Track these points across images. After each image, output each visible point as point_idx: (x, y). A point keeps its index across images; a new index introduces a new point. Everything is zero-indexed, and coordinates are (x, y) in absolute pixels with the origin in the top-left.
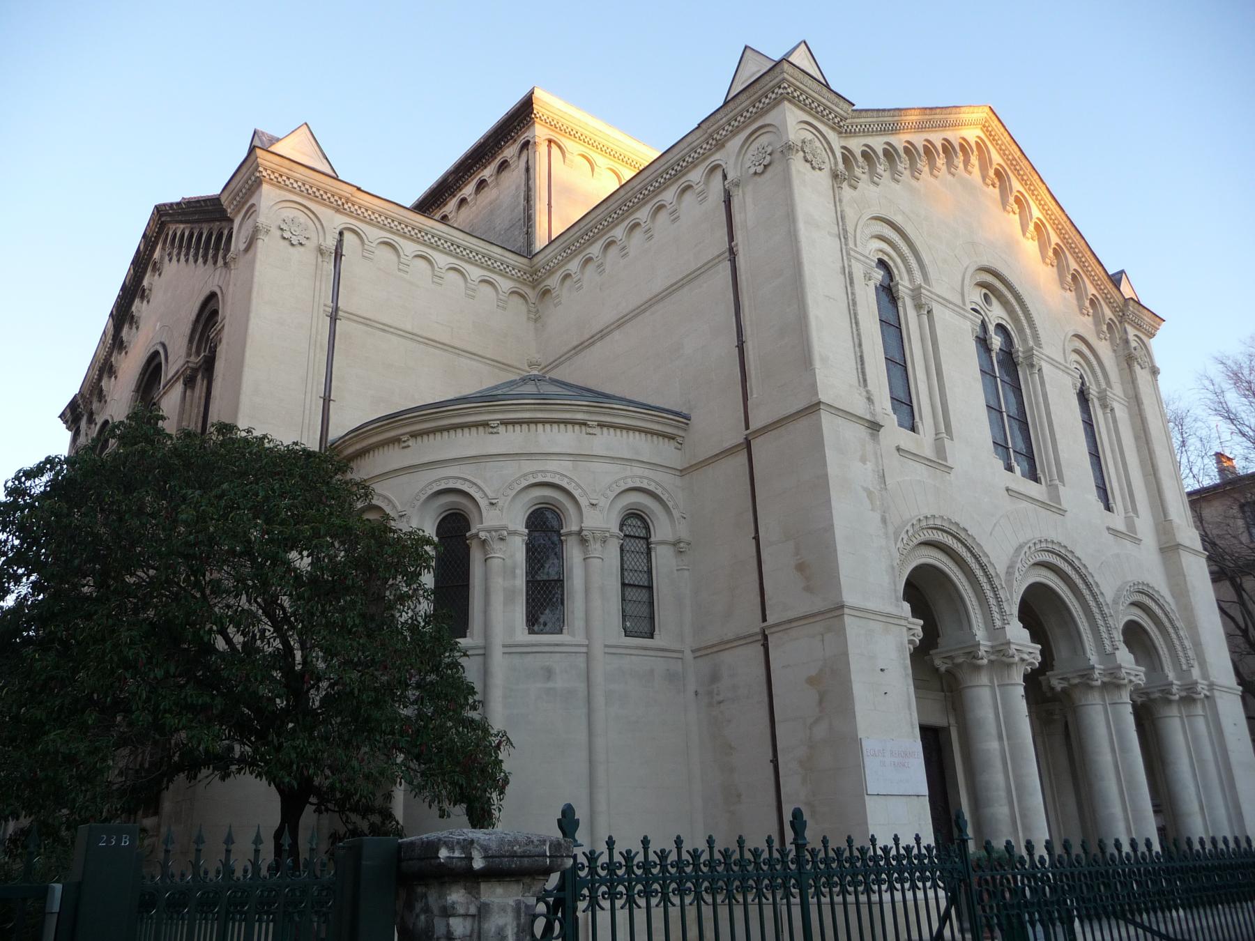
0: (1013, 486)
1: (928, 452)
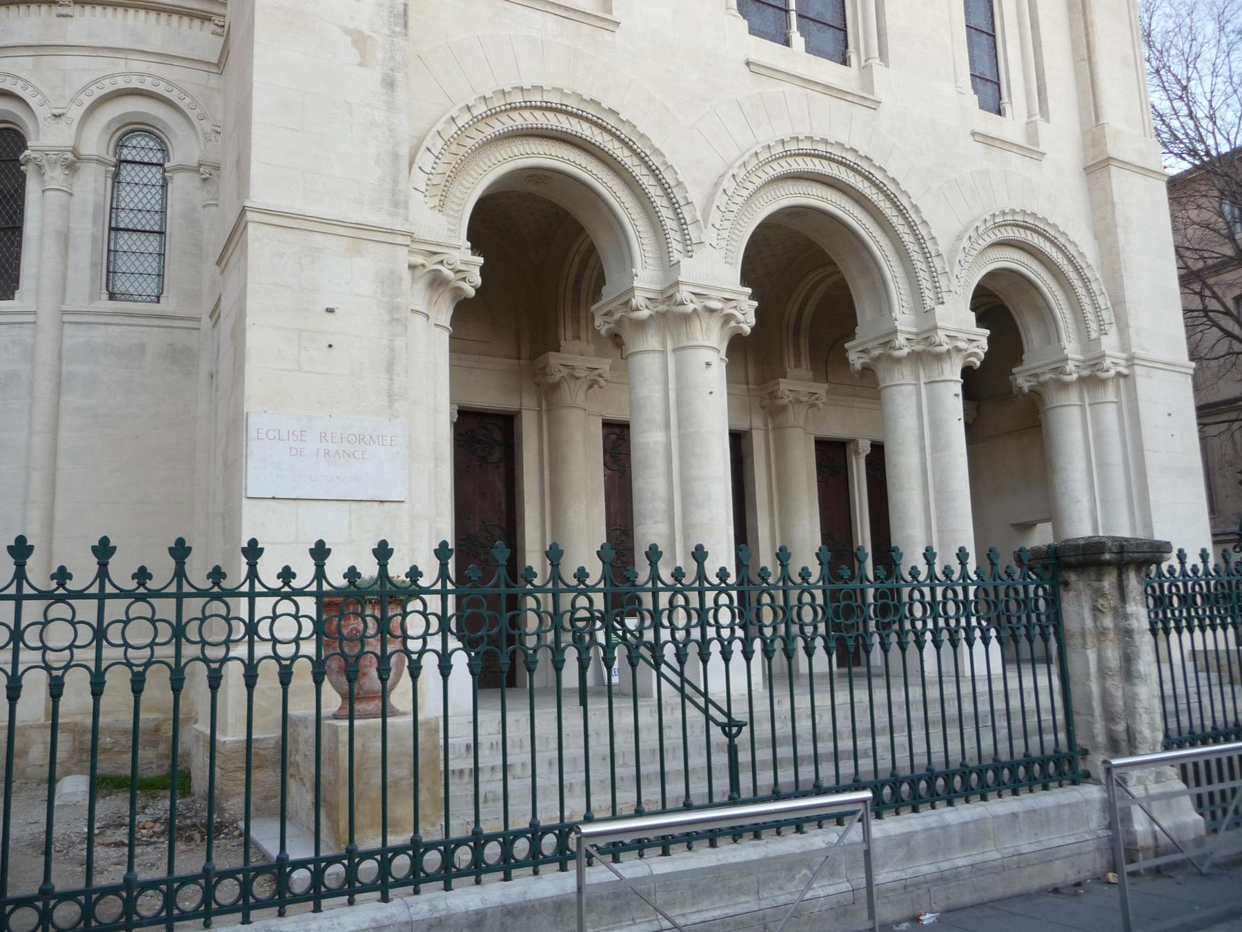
0: (753, 58)
1: (1020, 139)
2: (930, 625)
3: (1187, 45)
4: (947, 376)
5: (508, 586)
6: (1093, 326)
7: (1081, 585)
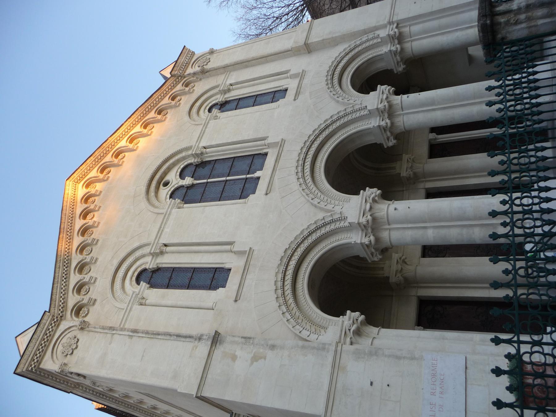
0: (264, 192)
1: (296, 81)
2: (532, 153)
3: (261, 20)
4: (399, 101)
5: (514, 310)
6: (375, 41)
7: (503, 32)
